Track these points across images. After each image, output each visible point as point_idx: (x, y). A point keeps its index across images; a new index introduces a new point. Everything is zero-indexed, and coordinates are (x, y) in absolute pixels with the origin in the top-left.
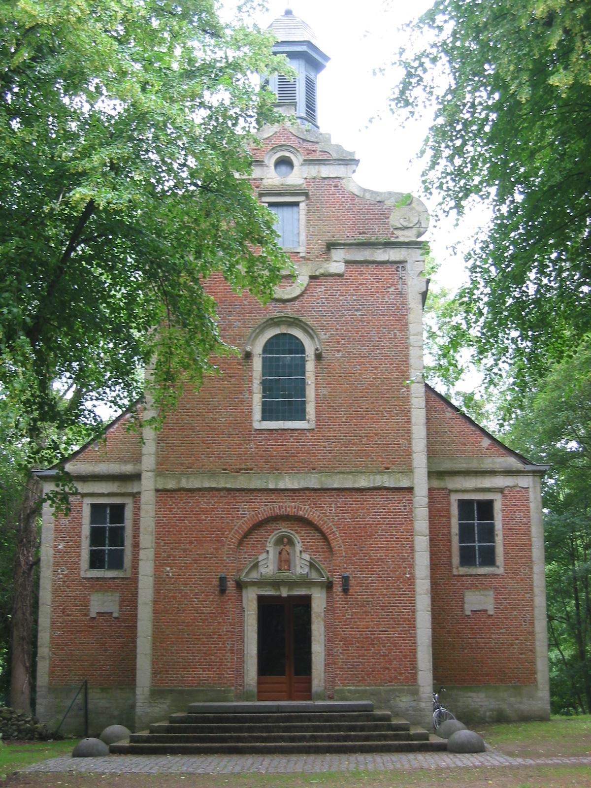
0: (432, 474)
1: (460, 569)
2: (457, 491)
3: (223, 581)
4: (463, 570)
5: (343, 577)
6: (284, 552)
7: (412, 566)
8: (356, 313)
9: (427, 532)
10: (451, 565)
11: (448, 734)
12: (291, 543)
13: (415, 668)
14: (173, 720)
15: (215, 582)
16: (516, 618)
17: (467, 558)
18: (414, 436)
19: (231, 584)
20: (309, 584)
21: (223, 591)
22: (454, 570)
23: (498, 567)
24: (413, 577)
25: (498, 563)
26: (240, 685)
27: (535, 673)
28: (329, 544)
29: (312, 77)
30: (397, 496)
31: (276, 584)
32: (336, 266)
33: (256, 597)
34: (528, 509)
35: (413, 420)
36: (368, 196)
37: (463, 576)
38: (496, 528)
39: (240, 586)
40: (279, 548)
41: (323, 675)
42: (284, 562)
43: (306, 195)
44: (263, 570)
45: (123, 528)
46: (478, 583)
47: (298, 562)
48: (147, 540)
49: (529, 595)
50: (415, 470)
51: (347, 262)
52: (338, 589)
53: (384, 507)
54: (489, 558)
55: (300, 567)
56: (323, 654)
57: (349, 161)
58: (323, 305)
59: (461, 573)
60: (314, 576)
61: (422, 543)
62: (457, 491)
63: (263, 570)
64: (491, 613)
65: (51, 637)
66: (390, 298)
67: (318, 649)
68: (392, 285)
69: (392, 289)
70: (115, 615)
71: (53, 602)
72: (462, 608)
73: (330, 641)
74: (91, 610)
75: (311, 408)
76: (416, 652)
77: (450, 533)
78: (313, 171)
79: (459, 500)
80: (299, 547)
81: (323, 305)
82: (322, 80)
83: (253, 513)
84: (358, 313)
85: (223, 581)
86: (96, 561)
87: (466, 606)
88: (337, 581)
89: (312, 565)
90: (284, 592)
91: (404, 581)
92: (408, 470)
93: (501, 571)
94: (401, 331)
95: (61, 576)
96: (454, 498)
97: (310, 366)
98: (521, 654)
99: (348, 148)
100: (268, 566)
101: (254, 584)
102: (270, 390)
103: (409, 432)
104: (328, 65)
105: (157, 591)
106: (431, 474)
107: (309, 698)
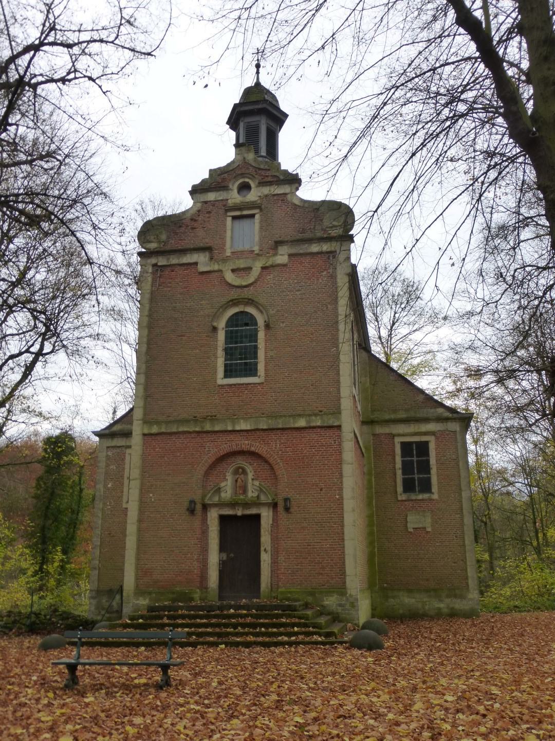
6: (239, 480)
7: (341, 489)
12: (244, 472)
19: (199, 507)
23: (433, 493)
24: (342, 498)
30: (329, 432)
31: (233, 504)
39: (205, 507)
44: (223, 495)
64: (429, 529)
67: (265, 558)
77: (394, 467)
95: (109, 507)
97: (261, 335)
101: (215, 505)
103: (338, 382)
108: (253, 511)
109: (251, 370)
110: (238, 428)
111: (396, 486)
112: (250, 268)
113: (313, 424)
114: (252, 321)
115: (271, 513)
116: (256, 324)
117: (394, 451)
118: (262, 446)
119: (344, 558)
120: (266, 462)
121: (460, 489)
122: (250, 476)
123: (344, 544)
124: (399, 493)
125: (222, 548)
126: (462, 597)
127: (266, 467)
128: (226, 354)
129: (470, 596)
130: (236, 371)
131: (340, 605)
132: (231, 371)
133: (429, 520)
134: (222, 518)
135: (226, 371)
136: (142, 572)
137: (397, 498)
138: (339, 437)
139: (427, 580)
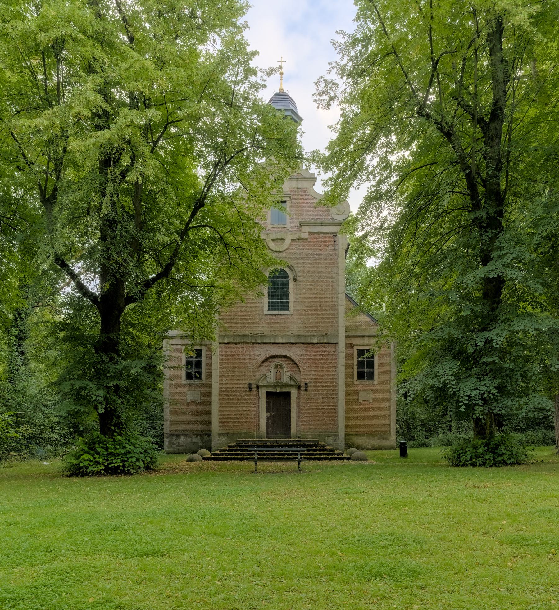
0: (347, 336)
2: (357, 345)
3: (250, 384)
6: (278, 372)
11: (352, 453)
12: (282, 367)
14: (229, 446)
17: (361, 376)
19: (254, 387)
20: (290, 386)
21: (250, 389)
28: (299, 368)
30: (330, 347)
31: (274, 386)
32: (305, 235)
35: (339, 311)
38: (375, 363)
39: (258, 387)
40: (276, 370)
42: (278, 376)
43: (290, 197)
44: (268, 380)
47: (285, 377)
48: (215, 365)
51: (310, 233)
52: (303, 388)
55: (285, 379)
60: (292, 383)
62: (357, 345)
63: (268, 380)
64: (371, 401)
65: (170, 411)
67: (293, 415)
70: (199, 401)
73: (298, 414)
75: (291, 305)
78: (294, 184)
80: (285, 370)
85: (250, 384)
88: (302, 385)
89: (291, 378)
90: (278, 390)
96: (356, 348)
97: (291, 284)
100: (271, 379)
101: (264, 386)
102: (272, 296)
105: (220, 389)
107: (290, 437)
108: (286, 390)
109: (286, 307)
110: (277, 342)
111: (353, 375)
112: (284, 240)
113: (322, 341)
114: (286, 276)
116: (288, 277)
117: (353, 354)
121: (390, 378)
125: (268, 410)
126: (387, 439)
128: (269, 295)
129: (391, 439)
130: (275, 306)
131: (335, 441)
132: (272, 306)
133: (372, 396)
134: (269, 394)
135: (269, 306)
136: (222, 423)
137: (354, 382)
139: (368, 429)
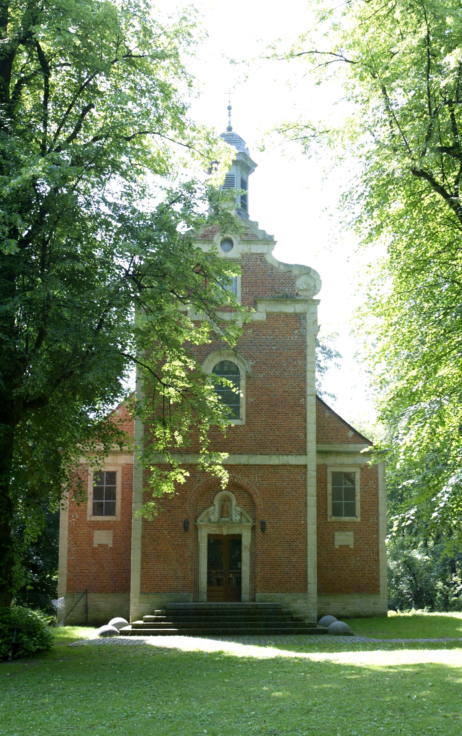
1: (333, 517)
4: (334, 518)
5: (262, 523)
7: (306, 516)
8: (273, 348)
9: (315, 494)
10: (327, 515)
13: (306, 581)
15: (181, 525)
16: (367, 550)
17: (337, 512)
18: (308, 431)
22: (329, 518)
23: (356, 517)
24: (306, 523)
25: (357, 514)
26: (197, 592)
27: (379, 587)
29: (245, 178)
33: (206, 534)
34: (377, 478)
36: (282, 267)
37: (334, 522)
41: (248, 585)
45: (115, 488)
46: (343, 527)
47: (234, 513)
49: (375, 536)
50: (308, 454)
53: (288, 477)
54: (351, 512)
56: (249, 572)
57: (269, 241)
58: (252, 342)
59: (333, 520)
61: (312, 501)
65: (68, 560)
66: (294, 338)
68: (296, 329)
69: (296, 331)
71: (69, 536)
72: (333, 543)
73: (253, 564)
74: (94, 542)
76: (307, 572)
77: (326, 493)
79: (333, 472)
81: (252, 342)
82: (252, 179)
83: (205, 480)
84: (274, 348)
86: (98, 509)
87: (336, 543)
91: (300, 526)
92: (304, 451)
93: (358, 520)
94: (301, 360)
95: (74, 520)
98: (370, 574)
99: (269, 232)
103: (305, 428)
104: (256, 169)
106: (319, 452)
107: (240, 601)
115: (250, 534)
118: (244, 478)
119: (307, 569)
120: (246, 491)
122: (234, 502)
123: (307, 560)
124: (329, 516)
127: (246, 495)
138: (305, 474)
